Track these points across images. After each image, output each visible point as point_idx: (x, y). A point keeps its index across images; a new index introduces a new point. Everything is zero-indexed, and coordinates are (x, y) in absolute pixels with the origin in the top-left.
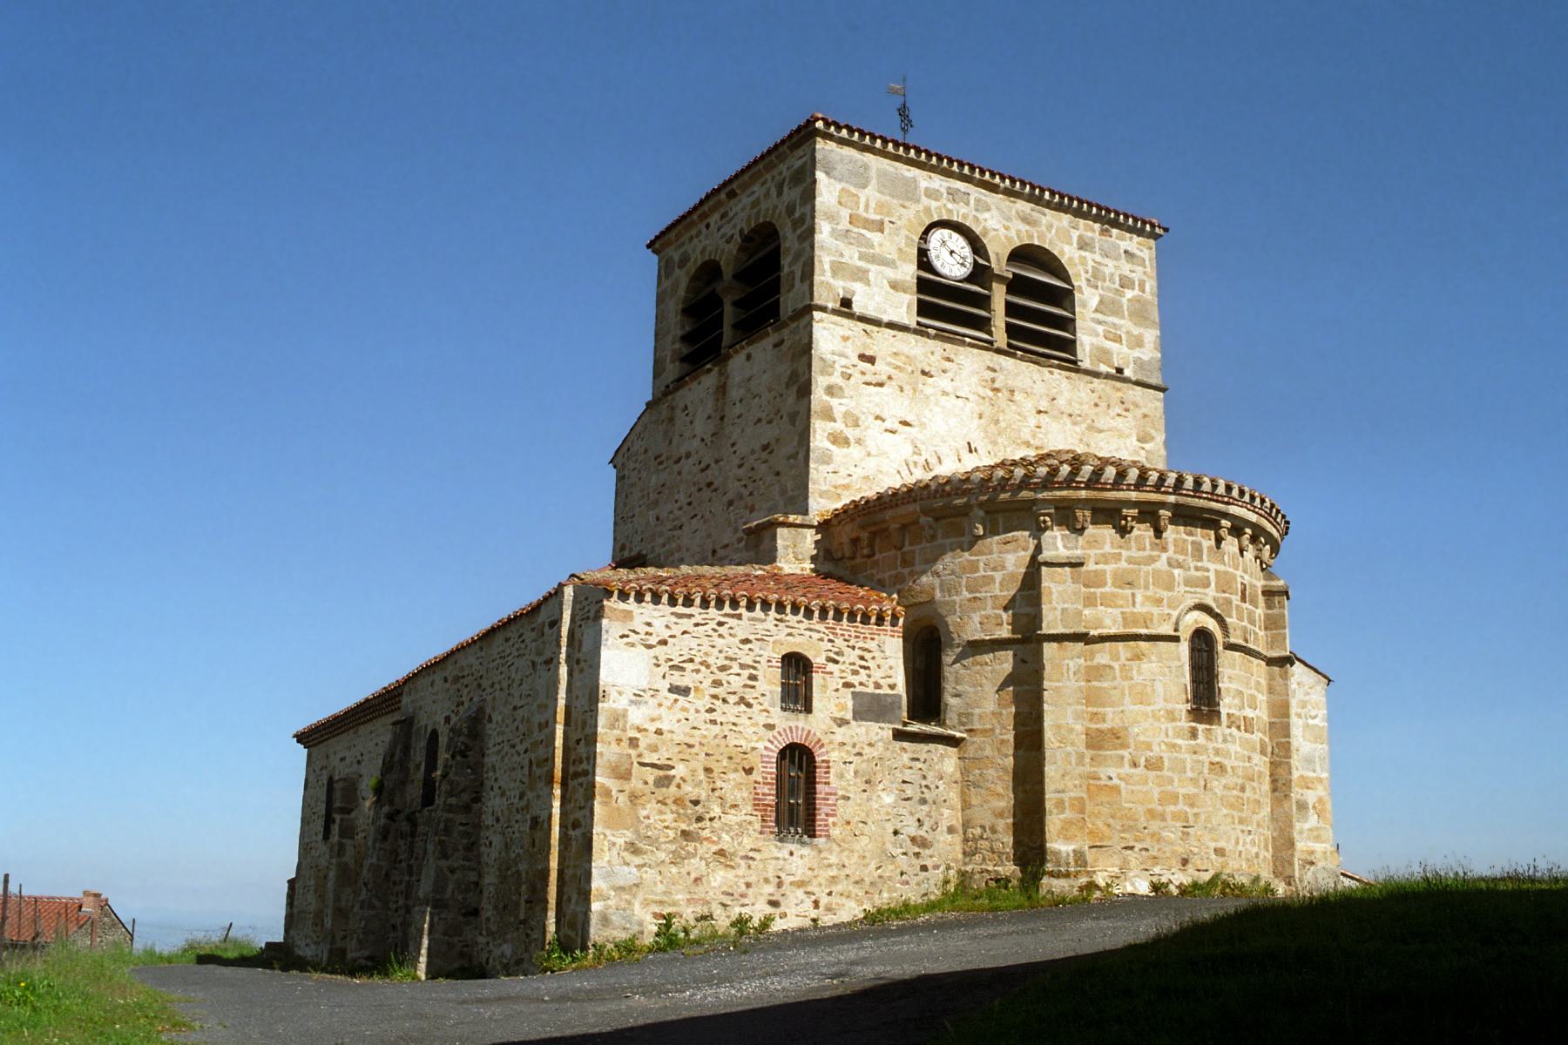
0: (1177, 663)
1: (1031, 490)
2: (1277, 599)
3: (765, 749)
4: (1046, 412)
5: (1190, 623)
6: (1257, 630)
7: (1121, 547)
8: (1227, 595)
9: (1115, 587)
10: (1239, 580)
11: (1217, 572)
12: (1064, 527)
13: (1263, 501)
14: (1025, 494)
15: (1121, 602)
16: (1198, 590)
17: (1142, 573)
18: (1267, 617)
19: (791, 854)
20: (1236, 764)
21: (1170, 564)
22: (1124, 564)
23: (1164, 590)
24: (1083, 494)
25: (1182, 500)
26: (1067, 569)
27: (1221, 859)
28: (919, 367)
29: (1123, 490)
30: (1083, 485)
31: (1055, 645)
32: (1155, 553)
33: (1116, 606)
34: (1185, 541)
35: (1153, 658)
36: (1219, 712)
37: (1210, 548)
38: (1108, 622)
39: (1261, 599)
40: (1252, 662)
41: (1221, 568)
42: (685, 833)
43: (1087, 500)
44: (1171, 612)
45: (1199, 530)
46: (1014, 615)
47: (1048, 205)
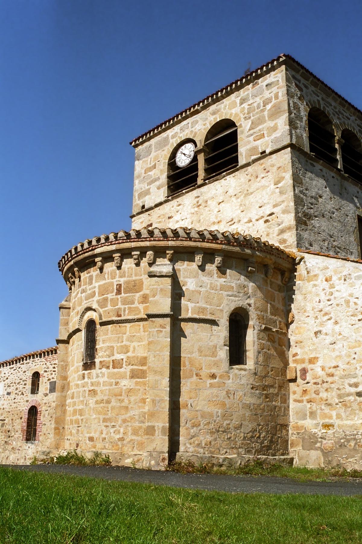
3: (25, 408)
4: (223, 201)
19: (29, 447)
20: (104, 388)
27: (91, 443)
36: (95, 362)
42: (6, 442)
47: (223, 97)
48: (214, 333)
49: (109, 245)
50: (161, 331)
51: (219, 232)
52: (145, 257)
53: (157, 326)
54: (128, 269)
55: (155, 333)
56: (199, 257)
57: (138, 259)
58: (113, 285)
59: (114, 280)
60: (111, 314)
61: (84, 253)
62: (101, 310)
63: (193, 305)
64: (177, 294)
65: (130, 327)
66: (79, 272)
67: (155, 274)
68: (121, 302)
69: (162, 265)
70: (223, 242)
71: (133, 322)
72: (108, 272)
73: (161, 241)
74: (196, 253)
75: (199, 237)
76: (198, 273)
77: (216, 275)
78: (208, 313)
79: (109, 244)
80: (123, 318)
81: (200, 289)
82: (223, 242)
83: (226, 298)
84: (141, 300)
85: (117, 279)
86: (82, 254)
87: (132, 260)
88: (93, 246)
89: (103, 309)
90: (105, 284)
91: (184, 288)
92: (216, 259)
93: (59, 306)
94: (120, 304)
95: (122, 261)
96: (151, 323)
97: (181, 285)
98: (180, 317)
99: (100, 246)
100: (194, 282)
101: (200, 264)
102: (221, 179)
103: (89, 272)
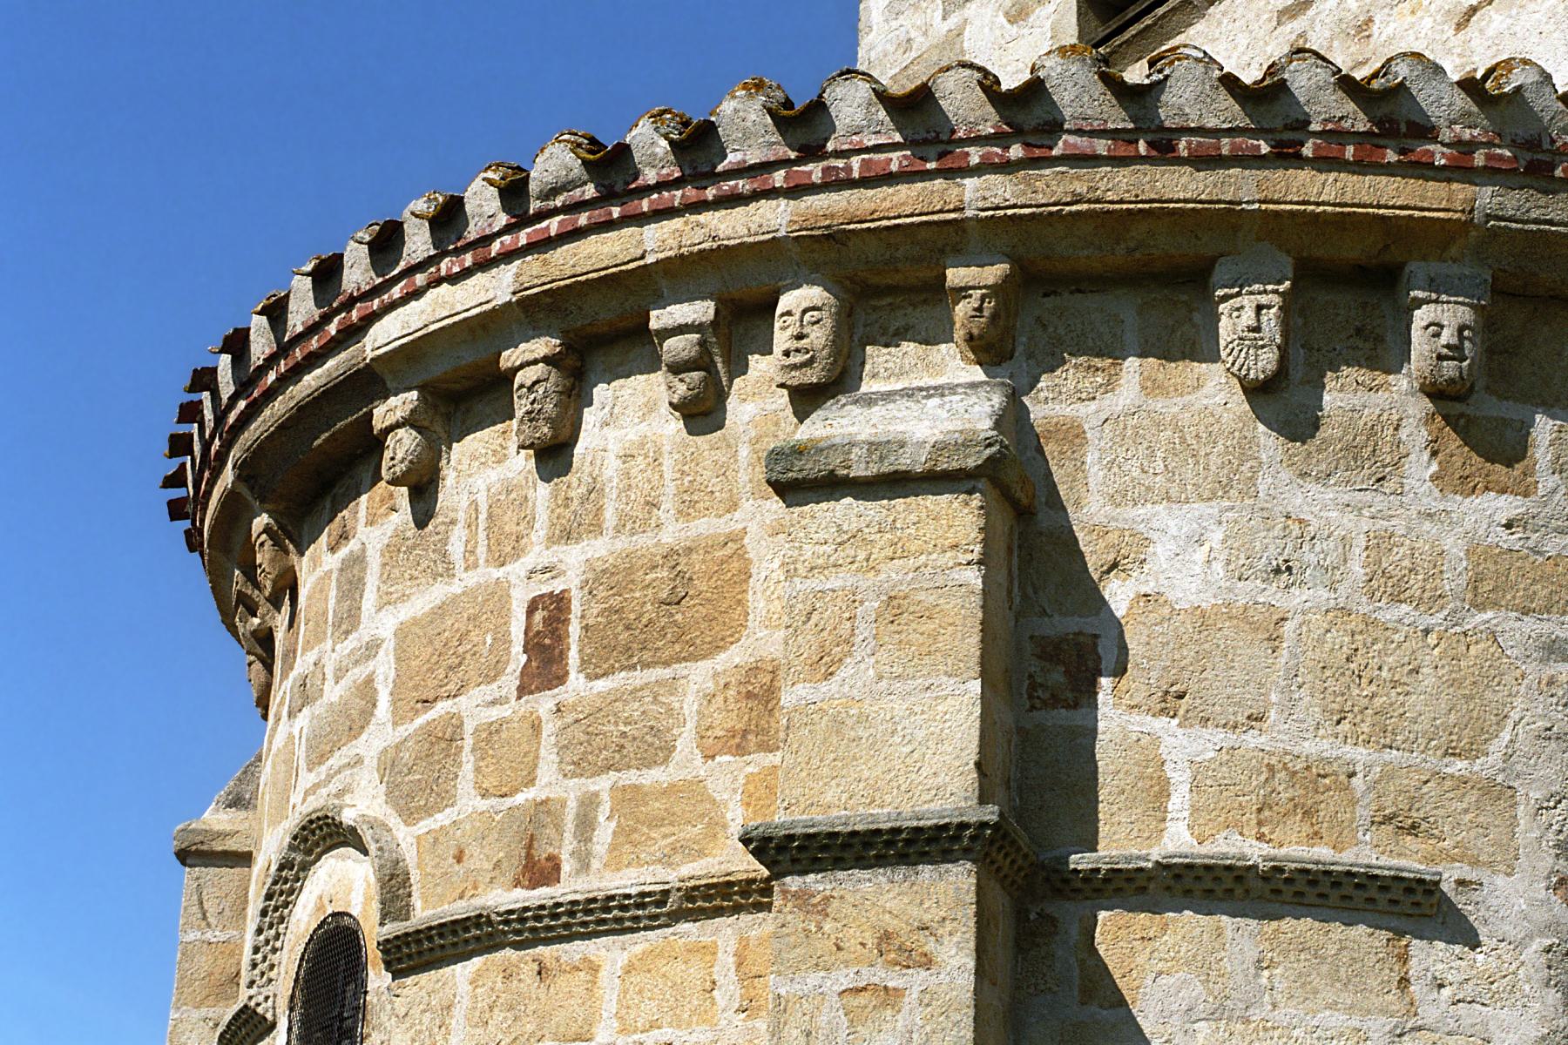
48: (1428, 1014)
49: (466, 273)
50: (890, 996)
51: (1438, 70)
52: (767, 350)
53: (851, 944)
54: (627, 457)
55: (831, 1015)
56: (1249, 302)
57: (701, 362)
58: (503, 612)
59: (516, 569)
60: (478, 859)
61: (296, 372)
62: (406, 838)
63: (1206, 743)
64: (1051, 651)
65: (629, 969)
66: (278, 543)
67: (835, 461)
68: (562, 749)
69: (908, 393)
70: (1479, 159)
71: (654, 923)
72: (474, 504)
73: (889, 179)
74: (1219, 273)
75: (1243, 121)
76: (1245, 450)
77: (1420, 469)
78: (1363, 813)
79: (468, 259)
80: (570, 888)
81: (1272, 594)
82: (1479, 159)
84: (723, 722)
85: (536, 554)
86: (285, 381)
87: (659, 378)
88: (351, 302)
89: (425, 825)
90: (440, 611)
91: (1119, 595)
92: (1421, 316)
93: (175, 845)
94: (547, 770)
95: (575, 395)
96: (795, 920)
97: (1094, 563)
98: (1080, 861)
99: (396, 292)
100: (1216, 536)
101: (1265, 362)
103: (344, 536)
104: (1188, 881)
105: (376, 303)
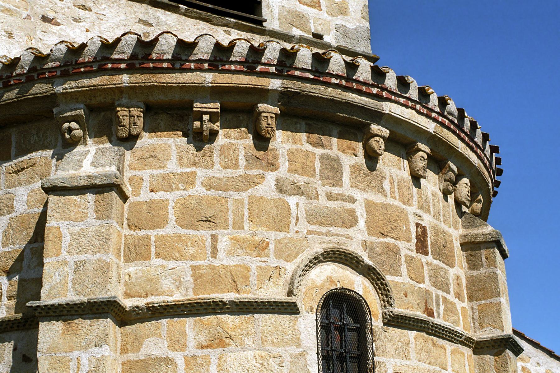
0: (294, 350)
1: (47, 81)
2: (484, 253)
5: (319, 282)
6: (451, 297)
7: (195, 164)
8: (388, 240)
9: (182, 227)
10: (413, 221)
11: (369, 206)
12: (105, 138)
13: (443, 102)
14: (39, 89)
15: (192, 250)
16: (333, 229)
17: (230, 204)
18: (471, 281)
21: (280, 189)
22: (199, 190)
23: (269, 228)
24: (125, 79)
25: (294, 86)
26: (90, 197)
28: (40, 12)
29: (190, 70)
30: (123, 66)
31: (58, 326)
32: (254, 172)
33: (183, 257)
34: (307, 154)
35: (248, 342)
37: (355, 168)
38: (167, 284)
39: (459, 254)
40: (442, 347)
41: (378, 199)
43: (132, 89)
44: (281, 263)
45: (335, 140)
46: (21, 282)
49: (422, 114)
83: (131, 199)
99: (402, 100)
102: (217, 25)
104: (94, 309)
105: (393, 98)
